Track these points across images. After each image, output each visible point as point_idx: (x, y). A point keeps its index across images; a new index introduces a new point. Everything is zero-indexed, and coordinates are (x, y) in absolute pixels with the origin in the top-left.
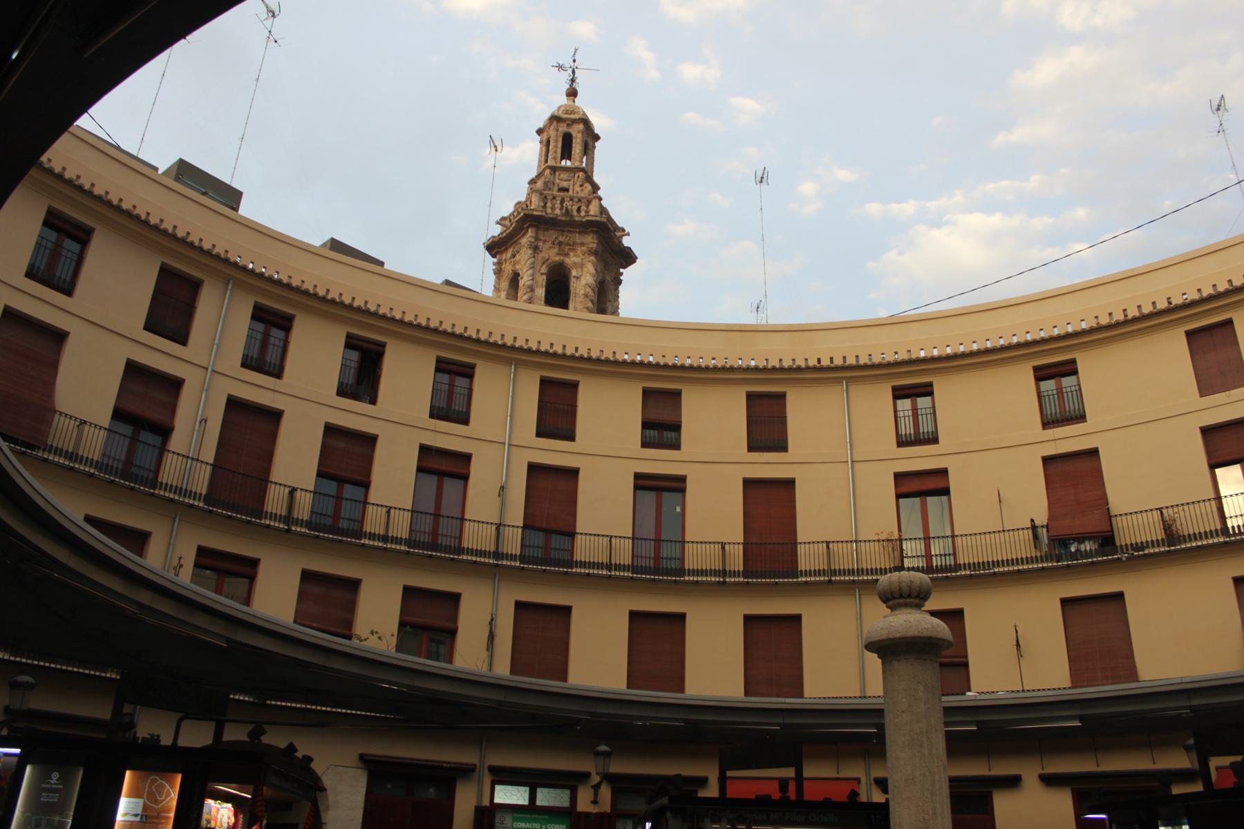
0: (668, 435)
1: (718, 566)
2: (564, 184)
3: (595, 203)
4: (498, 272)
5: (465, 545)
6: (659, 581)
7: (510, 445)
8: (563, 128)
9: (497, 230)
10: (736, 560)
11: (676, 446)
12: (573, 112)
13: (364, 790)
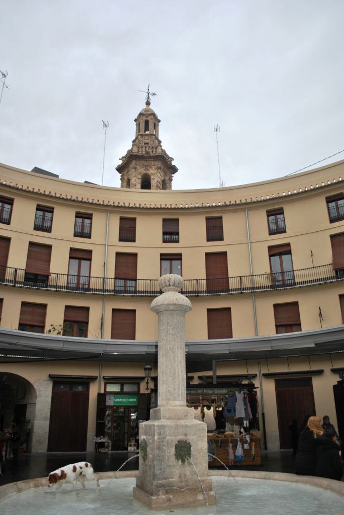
0: (174, 237)
1: (195, 289)
2: (147, 141)
3: (159, 148)
4: (122, 179)
5: (91, 287)
6: (29, 288)
7: (105, 245)
8: (145, 118)
9: (120, 162)
10: (203, 286)
11: (177, 241)
12: (148, 111)
13: (51, 389)
